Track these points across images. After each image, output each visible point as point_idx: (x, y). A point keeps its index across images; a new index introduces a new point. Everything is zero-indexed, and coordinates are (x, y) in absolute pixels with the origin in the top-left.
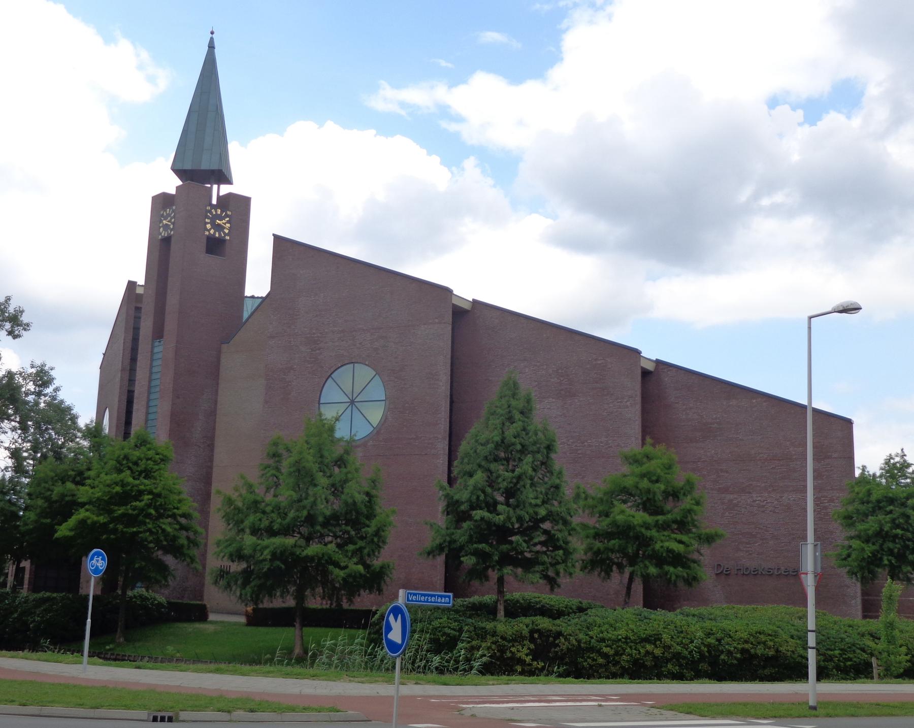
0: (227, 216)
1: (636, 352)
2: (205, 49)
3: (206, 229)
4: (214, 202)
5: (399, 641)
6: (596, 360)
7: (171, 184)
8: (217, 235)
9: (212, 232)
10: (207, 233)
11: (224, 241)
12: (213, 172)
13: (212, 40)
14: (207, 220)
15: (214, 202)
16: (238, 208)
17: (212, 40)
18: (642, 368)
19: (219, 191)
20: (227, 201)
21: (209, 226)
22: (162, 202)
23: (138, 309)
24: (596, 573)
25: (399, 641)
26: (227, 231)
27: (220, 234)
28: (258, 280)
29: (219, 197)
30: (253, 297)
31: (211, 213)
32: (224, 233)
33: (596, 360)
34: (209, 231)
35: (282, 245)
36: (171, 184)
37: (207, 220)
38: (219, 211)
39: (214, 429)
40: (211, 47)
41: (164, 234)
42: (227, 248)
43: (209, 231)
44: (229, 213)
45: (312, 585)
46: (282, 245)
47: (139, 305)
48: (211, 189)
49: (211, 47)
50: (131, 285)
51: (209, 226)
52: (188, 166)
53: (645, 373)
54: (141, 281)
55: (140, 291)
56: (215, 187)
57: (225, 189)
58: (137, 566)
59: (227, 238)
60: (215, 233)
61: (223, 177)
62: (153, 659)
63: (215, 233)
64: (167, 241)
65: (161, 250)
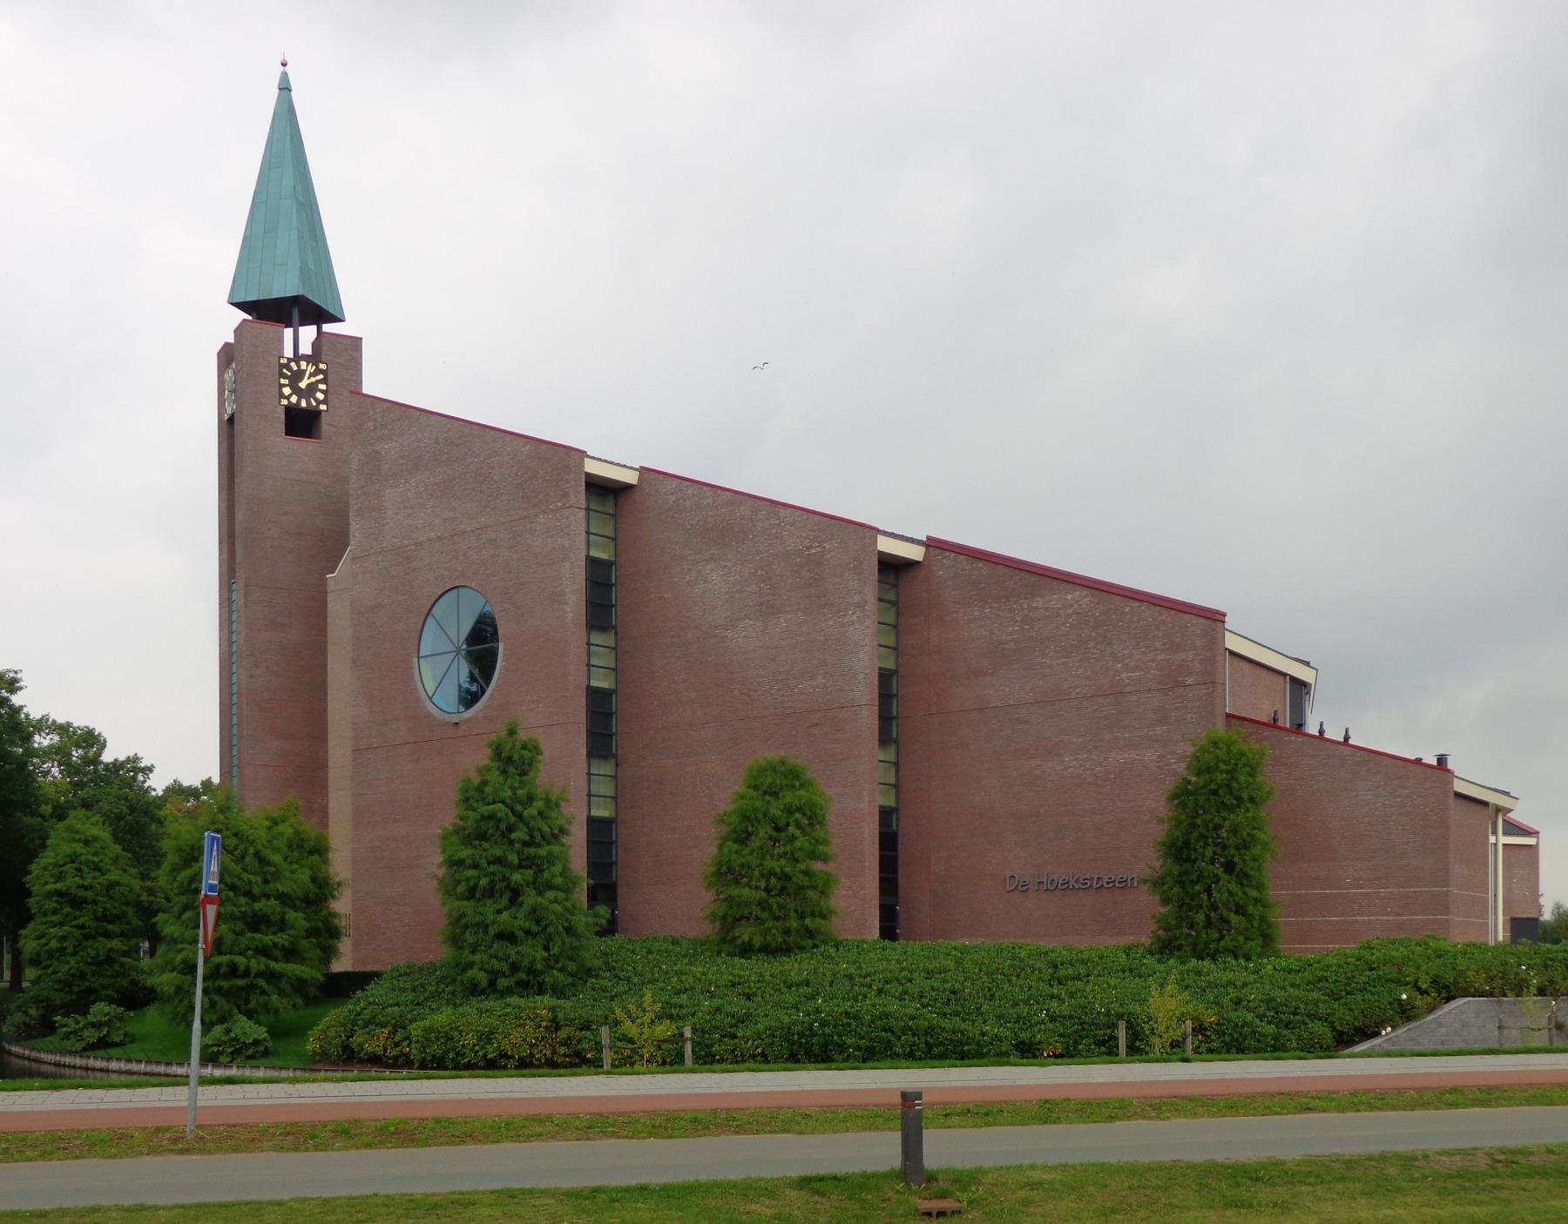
1: (227, 356)
3: (282, 396)
6: (809, 548)
8: (304, 404)
9: (294, 399)
10: (285, 402)
11: (318, 413)
13: (285, 76)
14: (283, 381)
17: (285, 76)
18: (588, 475)
21: (287, 391)
22: (227, 345)
24: (826, 849)
27: (308, 402)
31: (290, 369)
32: (317, 400)
33: (809, 548)
34: (288, 398)
37: (283, 381)
40: (285, 88)
43: (288, 398)
44: (322, 366)
45: (531, 946)
49: (285, 88)
51: (287, 391)
52: (253, 297)
53: (892, 567)
59: (323, 407)
60: (299, 401)
63: (299, 401)
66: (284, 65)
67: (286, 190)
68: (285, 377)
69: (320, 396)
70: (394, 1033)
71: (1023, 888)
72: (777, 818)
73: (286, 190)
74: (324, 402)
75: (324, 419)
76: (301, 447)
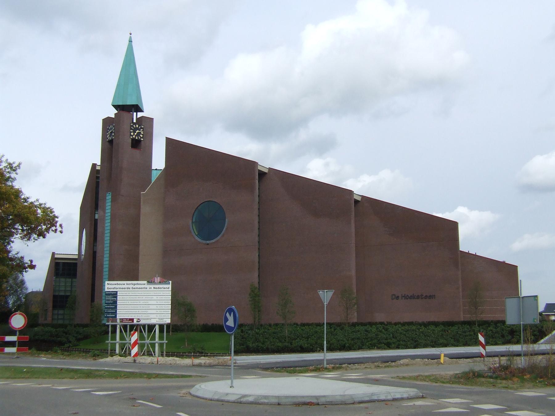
0: (141, 128)
2: (127, 42)
4: (135, 121)
5: (233, 326)
7: (112, 112)
11: (141, 141)
12: (133, 106)
13: (130, 37)
15: (135, 121)
16: (147, 124)
17: (130, 37)
19: (136, 116)
20: (140, 120)
21: (132, 134)
22: (107, 122)
23: (98, 178)
25: (233, 326)
26: (141, 136)
28: (159, 161)
29: (137, 119)
30: (156, 169)
34: (132, 136)
35: (171, 144)
36: (112, 112)
38: (137, 126)
39: (275, 396)
40: (130, 41)
41: (110, 138)
42: (141, 144)
43: (132, 136)
46: (171, 144)
47: (98, 175)
48: (133, 114)
49: (130, 41)
50: (94, 165)
51: (132, 134)
54: (99, 163)
55: (98, 168)
56: (135, 114)
57: (140, 115)
58: (35, 280)
61: (138, 108)
62: (80, 351)
64: (111, 142)
65: (109, 146)
66: (131, 34)
67: (129, 74)
68: (132, 129)
69: (141, 136)
70: (249, 330)
71: (397, 298)
72: (126, 331)
73: (129, 74)
74: (142, 138)
75: (142, 142)
76: (136, 152)
